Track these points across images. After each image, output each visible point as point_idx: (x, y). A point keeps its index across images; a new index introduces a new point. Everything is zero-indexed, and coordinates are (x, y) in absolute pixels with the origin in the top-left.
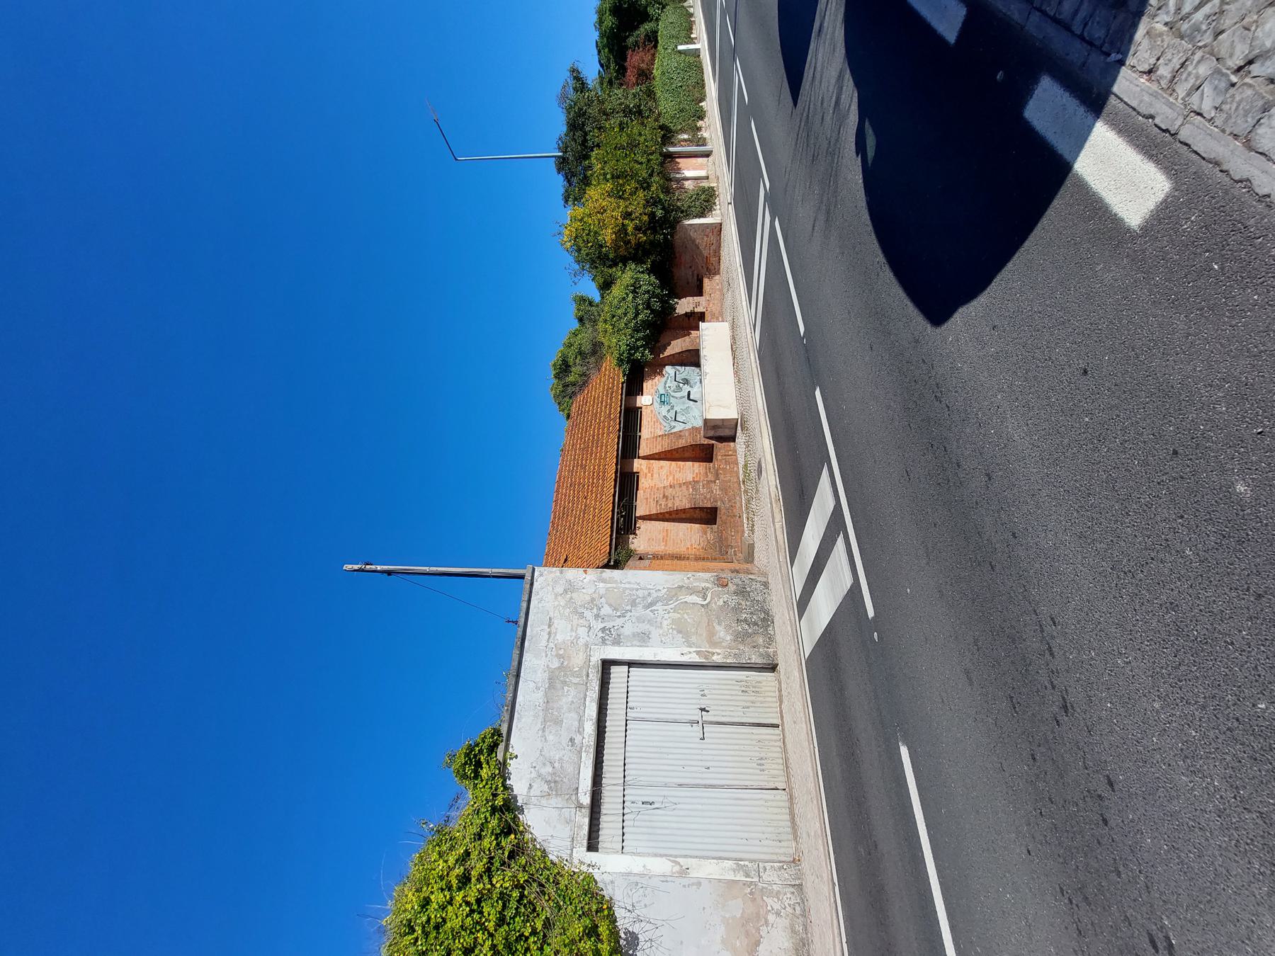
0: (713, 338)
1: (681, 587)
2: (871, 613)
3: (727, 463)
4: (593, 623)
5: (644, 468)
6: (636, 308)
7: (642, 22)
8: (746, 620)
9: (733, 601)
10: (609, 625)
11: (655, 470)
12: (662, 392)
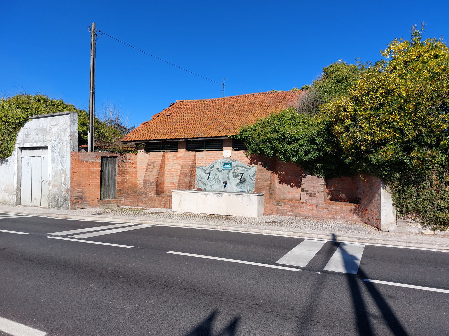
1: (66, 175)
4: (56, 141)
8: (58, 199)
9: (63, 195)
10: (56, 147)
11: (178, 161)
12: (233, 164)
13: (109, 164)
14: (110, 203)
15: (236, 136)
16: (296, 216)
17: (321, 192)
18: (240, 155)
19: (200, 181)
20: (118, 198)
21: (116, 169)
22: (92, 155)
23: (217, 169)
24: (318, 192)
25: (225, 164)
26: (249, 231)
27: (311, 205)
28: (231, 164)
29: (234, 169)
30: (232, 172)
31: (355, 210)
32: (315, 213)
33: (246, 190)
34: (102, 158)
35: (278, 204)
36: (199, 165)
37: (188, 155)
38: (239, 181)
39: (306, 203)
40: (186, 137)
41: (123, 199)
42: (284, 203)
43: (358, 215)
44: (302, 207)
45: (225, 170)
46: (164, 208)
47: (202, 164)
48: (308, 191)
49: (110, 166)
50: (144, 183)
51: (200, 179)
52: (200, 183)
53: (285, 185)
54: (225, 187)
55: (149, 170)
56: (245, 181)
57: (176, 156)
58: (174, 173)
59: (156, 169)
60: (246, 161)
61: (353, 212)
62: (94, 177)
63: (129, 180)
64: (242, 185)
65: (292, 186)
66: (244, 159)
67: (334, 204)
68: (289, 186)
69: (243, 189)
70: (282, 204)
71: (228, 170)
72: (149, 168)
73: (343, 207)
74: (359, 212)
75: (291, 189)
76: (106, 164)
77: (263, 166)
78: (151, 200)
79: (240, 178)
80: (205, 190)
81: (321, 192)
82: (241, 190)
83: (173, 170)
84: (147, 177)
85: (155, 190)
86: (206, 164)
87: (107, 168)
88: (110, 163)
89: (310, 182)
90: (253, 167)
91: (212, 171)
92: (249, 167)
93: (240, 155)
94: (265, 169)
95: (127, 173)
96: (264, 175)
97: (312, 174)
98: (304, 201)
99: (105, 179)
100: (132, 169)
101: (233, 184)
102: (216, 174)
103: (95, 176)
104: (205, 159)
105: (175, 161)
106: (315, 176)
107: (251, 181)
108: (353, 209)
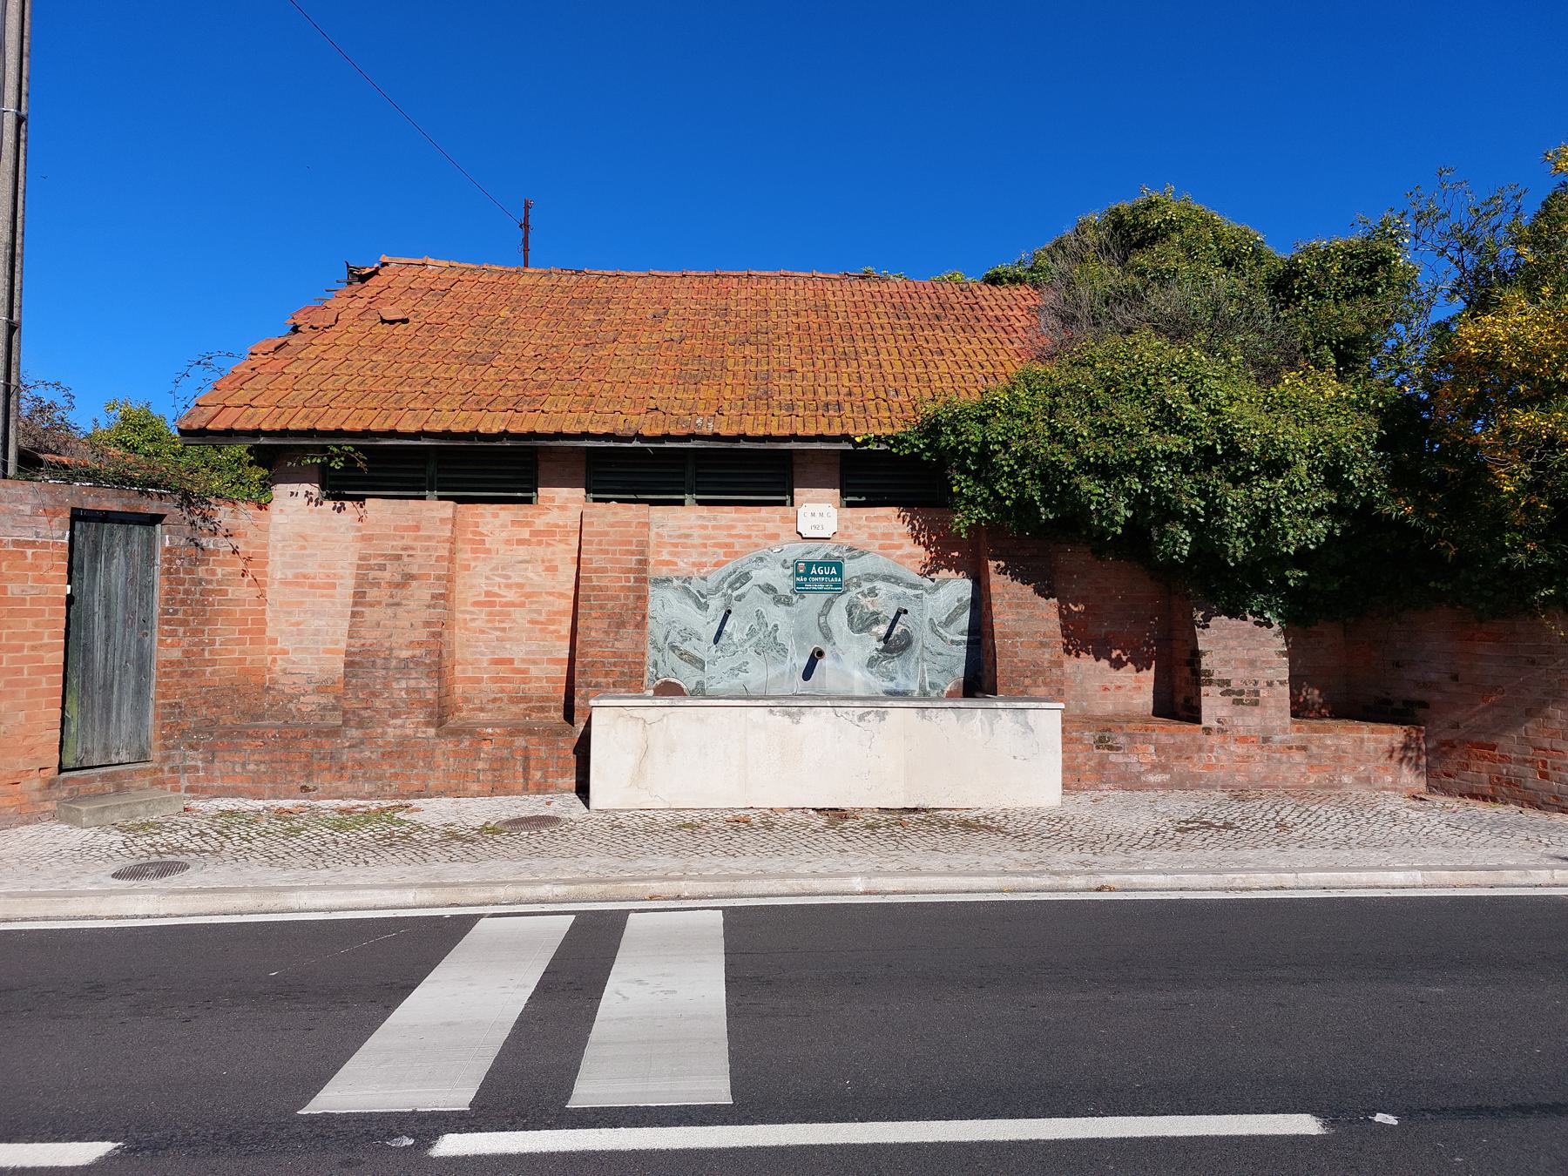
0: (1011, 758)
2: (1305, 1125)
3: (499, 764)
5: (554, 517)
6: (1128, 467)
7: (1386, 522)
12: (851, 568)
13: (109, 560)
14: (119, 789)
15: (899, 441)
16: (1182, 787)
17: (1282, 683)
18: (882, 527)
19: (673, 648)
20: (166, 759)
21: (150, 587)
22: (20, 500)
23: (769, 589)
24: (1270, 684)
25: (809, 565)
26: (1238, 883)
27: (1243, 740)
28: (839, 567)
29: (854, 592)
30: (842, 602)
31: (1406, 747)
32: (1258, 769)
33: (914, 687)
34: (78, 516)
35: (1101, 739)
36: (664, 572)
37: (611, 519)
38: (881, 645)
39: (1221, 731)
40: (621, 429)
41: (196, 759)
42: (1128, 735)
43: (1417, 766)
44: (1206, 747)
45: (810, 596)
46: (493, 792)
47: (683, 565)
48: (1228, 682)
49: (115, 572)
50: (348, 664)
51: (675, 637)
52: (673, 658)
53: (1086, 661)
54: (807, 674)
55: (373, 593)
56: (909, 643)
57: (529, 524)
58: (518, 614)
59: (421, 593)
60: (910, 556)
61: (1397, 755)
62: (27, 637)
63: (228, 651)
64: (895, 664)
65: (1117, 664)
66: (900, 547)
67: (1330, 731)
68: (1104, 663)
69: (901, 683)
70: (1122, 740)
71: (824, 597)
72: (376, 584)
73: (1362, 741)
74: (1419, 758)
75: (1113, 673)
76: (95, 556)
77: (1014, 577)
78: (401, 755)
79: (882, 630)
80: (700, 692)
81: (1282, 683)
82: (891, 686)
83: (511, 595)
84: (369, 636)
85: (428, 704)
86: (701, 565)
87: (100, 579)
88: (119, 552)
89: (1232, 643)
90: (947, 580)
91: (739, 599)
92: (927, 582)
93: (882, 527)
94: (1029, 590)
95: (218, 613)
96: (1032, 616)
97: (1233, 613)
98: (1215, 724)
99: (88, 650)
100: (242, 591)
101: (851, 660)
102: (759, 615)
103: (30, 628)
104: (697, 541)
105: (522, 552)
106: (1245, 619)
107: (940, 646)
108: (1397, 745)
